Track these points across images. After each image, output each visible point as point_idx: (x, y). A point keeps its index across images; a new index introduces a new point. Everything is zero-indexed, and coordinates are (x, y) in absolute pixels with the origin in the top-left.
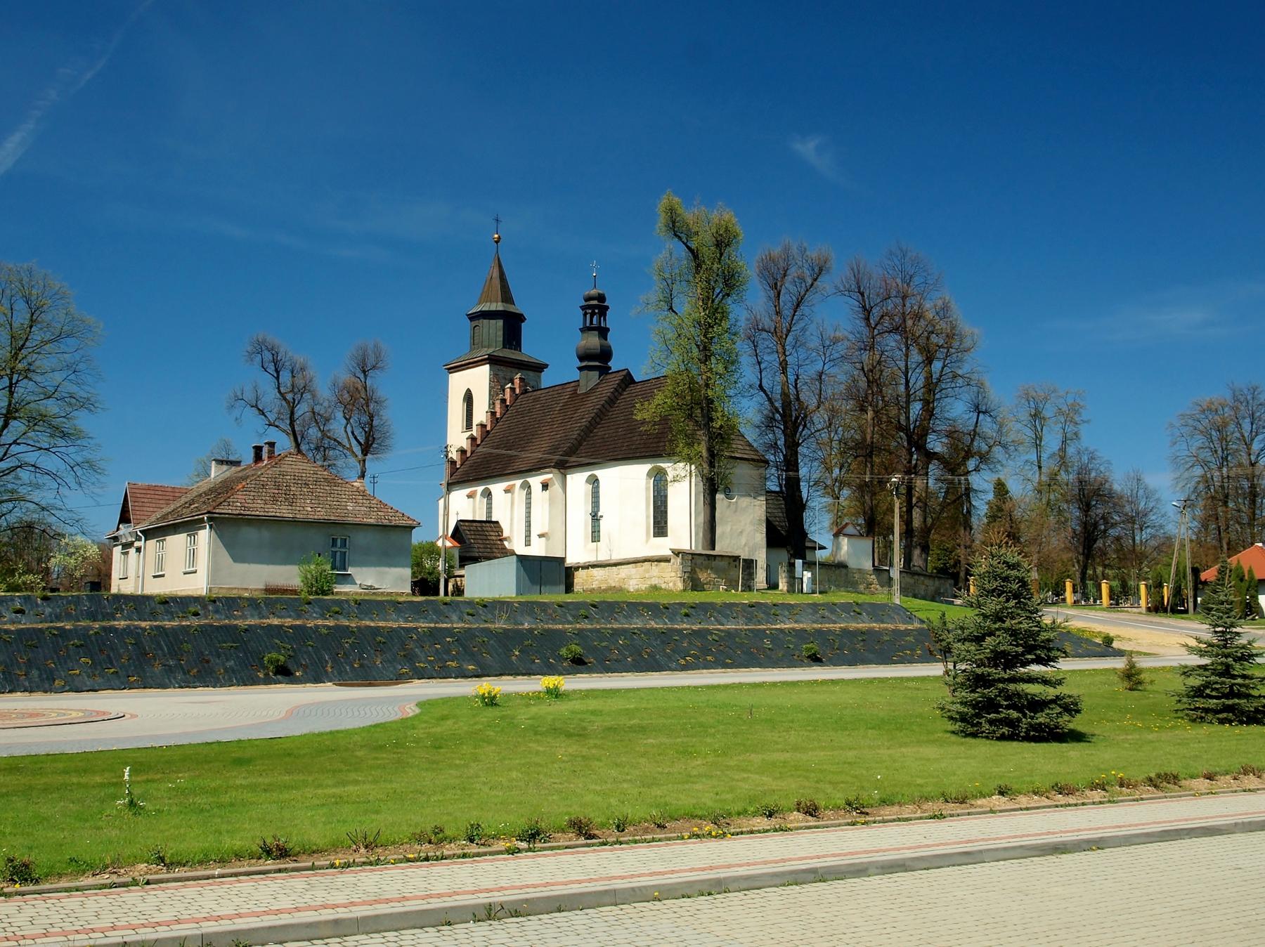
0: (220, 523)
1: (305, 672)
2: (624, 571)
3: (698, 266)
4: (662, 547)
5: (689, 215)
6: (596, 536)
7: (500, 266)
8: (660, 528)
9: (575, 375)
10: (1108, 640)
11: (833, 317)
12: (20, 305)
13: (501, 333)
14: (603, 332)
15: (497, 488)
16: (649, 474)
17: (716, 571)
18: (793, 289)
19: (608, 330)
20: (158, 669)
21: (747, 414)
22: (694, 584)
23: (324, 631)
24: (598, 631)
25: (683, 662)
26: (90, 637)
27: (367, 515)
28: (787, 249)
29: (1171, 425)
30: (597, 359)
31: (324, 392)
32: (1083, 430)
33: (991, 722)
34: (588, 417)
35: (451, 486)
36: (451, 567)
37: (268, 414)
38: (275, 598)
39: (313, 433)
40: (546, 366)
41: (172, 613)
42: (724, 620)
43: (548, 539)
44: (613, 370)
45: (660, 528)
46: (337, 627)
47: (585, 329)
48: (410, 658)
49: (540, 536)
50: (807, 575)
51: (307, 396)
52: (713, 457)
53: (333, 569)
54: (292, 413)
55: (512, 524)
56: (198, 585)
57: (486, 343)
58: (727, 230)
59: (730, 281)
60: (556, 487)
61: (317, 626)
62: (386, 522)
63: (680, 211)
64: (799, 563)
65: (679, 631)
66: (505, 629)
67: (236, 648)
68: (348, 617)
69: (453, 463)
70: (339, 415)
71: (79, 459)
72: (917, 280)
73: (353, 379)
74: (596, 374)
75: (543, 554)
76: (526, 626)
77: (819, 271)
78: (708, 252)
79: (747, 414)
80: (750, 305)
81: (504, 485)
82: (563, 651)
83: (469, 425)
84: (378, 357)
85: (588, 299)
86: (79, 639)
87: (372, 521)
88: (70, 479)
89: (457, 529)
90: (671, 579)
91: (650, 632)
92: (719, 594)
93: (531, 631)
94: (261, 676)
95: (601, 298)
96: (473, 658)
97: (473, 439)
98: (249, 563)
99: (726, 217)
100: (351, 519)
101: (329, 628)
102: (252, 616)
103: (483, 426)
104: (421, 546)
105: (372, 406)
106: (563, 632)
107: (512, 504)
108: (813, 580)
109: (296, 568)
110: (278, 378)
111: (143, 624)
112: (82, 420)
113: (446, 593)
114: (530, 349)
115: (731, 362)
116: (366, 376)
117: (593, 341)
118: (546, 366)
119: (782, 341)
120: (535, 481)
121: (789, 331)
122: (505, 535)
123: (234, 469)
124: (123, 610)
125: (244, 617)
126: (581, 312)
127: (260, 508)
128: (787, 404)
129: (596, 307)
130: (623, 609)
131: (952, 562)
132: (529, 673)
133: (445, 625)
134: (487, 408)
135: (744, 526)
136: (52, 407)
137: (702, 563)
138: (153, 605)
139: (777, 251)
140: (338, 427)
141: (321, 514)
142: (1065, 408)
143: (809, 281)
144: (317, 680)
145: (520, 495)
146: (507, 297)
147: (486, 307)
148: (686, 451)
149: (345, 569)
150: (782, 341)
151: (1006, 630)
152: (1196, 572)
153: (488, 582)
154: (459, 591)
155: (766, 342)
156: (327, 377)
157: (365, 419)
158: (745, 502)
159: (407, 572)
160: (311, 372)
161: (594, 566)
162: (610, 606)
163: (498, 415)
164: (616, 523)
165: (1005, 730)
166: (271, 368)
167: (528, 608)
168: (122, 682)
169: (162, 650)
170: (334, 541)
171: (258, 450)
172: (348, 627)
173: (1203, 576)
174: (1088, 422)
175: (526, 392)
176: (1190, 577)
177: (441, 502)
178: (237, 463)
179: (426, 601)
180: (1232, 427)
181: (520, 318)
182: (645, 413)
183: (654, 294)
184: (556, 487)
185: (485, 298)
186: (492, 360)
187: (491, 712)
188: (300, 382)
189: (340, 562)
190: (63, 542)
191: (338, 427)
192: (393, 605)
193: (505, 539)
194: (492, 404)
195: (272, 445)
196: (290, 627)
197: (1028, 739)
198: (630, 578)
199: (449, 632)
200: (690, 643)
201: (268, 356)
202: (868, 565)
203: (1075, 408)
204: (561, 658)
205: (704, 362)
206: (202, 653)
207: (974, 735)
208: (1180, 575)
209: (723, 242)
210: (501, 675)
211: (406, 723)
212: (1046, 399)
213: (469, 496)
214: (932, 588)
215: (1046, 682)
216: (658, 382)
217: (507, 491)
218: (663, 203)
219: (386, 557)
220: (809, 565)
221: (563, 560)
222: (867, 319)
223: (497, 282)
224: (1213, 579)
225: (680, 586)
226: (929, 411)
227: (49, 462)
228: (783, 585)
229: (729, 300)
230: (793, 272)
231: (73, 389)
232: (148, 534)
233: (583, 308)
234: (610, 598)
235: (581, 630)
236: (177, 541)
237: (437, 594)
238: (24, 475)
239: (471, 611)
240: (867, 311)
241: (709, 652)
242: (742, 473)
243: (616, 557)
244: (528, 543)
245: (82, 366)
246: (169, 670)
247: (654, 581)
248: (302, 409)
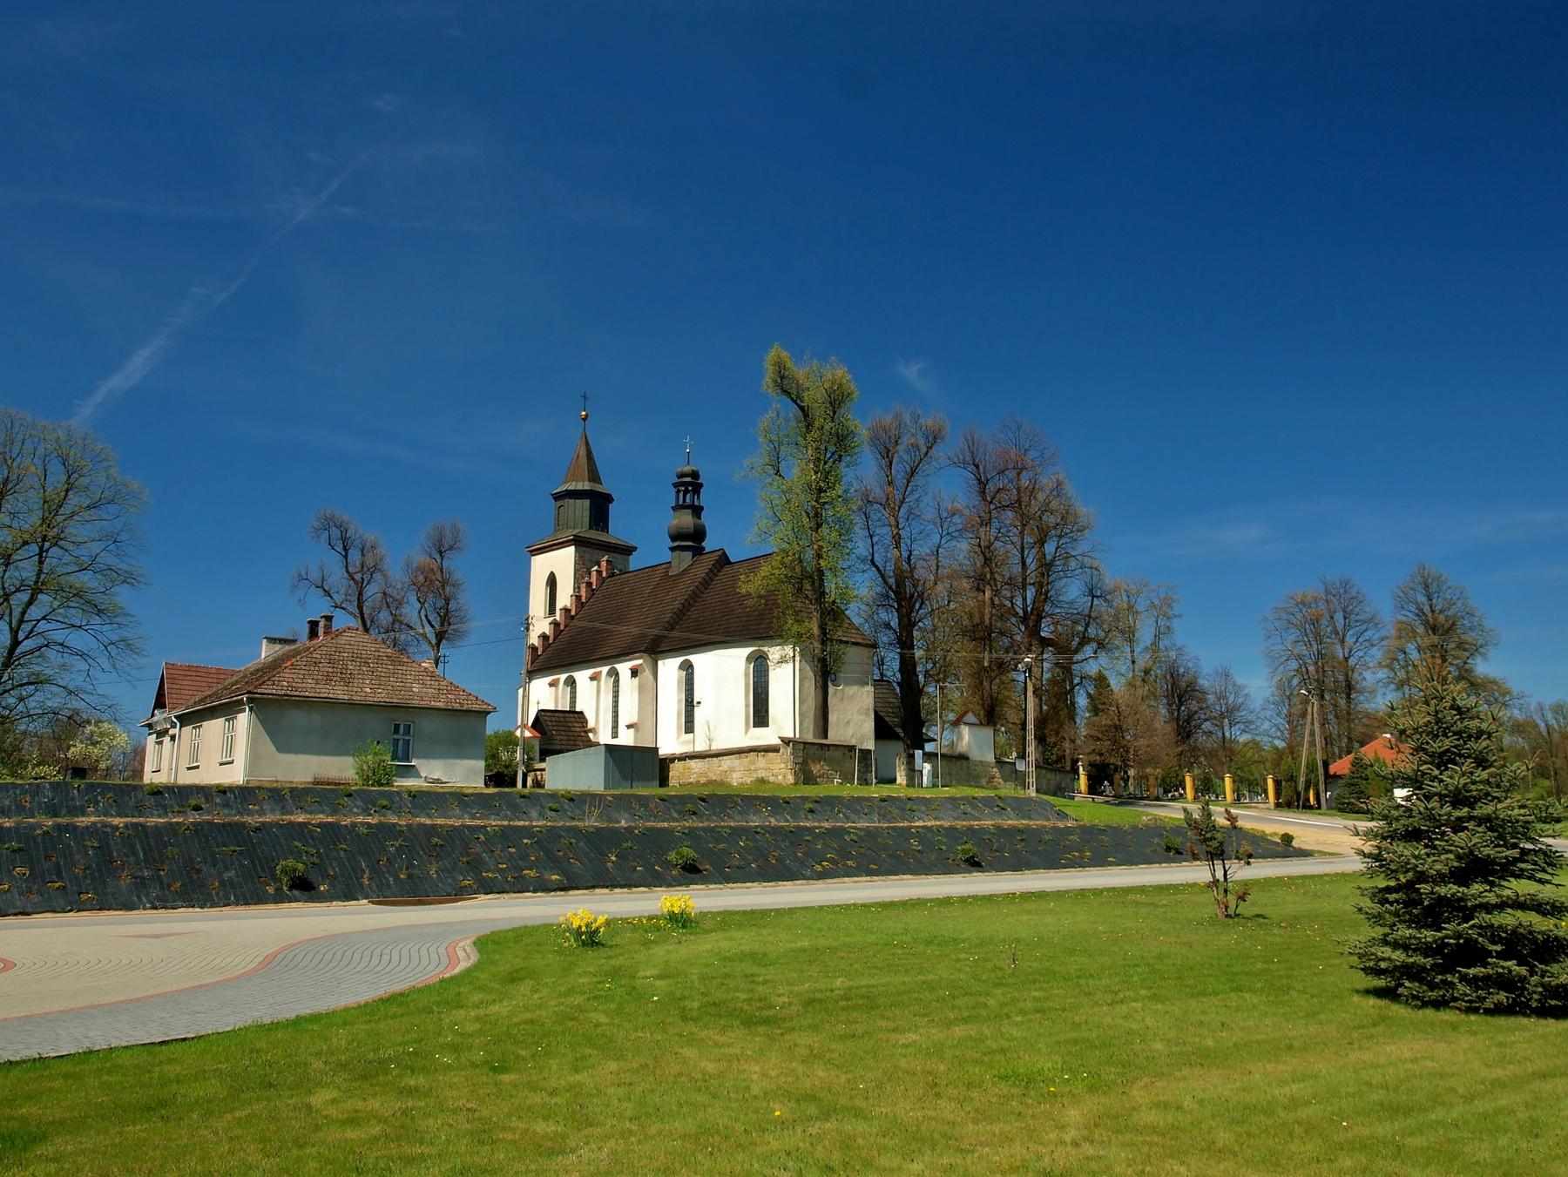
0: (260, 705)
1: (332, 885)
2: (727, 762)
3: (809, 426)
5: (800, 372)
7: (587, 444)
8: (761, 717)
9: (667, 556)
10: (1287, 839)
11: (947, 489)
12: (55, 467)
14: (697, 511)
15: (582, 676)
19: (702, 508)
20: (125, 881)
23: (364, 830)
24: (712, 830)
25: (819, 868)
26: (34, 838)
28: (898, 417)
29: (1266, 619)
31: (397, 574)
32: (1176, 624)
33: (1472, 982)
34: (681, 599)
35: (532, 674)
37: (335, 596)
38: (325, 793)
39: (385, 617)
41: (165, 808)
42: (853, 816)
45: (761, 717)
46: (381, 825)
48: (475, 866)
49: (629, 727)
50: (927, 767)
51: (377, 576)
52: (825, 639)
54: (360, 594)
56: (236, 775)
58: (840, 386)
59: (842, 441)
60: (647, 674)
61: (354, 825)
62: (457, 706)
63: (790, 364)
65: (810, 830)
66: (597, 828)
67: (240, 853)
68: (398, 813)
69: (534, 649)
70: (413, 598)
71: (114, 638)
75: (631, 743)
77: (934, 439)
78: (819, 412)
79: (859, 592)
80: (863, 472)
81: (590, 672)
82: (672, 856)
83: (552, 611)
84: (456, 539)
86: (19, 842)
87: (440, 705)
88: (103, 661)
90: (780, 772)
91: (774, 831)
92: (834, 787)
93: (629, 830)
94: (271, 890)
95: (695, 475)
96: (556, 863)
97: (556, 624)
98: (296, 752)
100: (415, 703)
101: (369, 825)
102: (273, 811)
103: (566, 610)
104: (497, 735)
106: (670, 831)
108: (934, 774)
109: (349, 760)
110: (346, 557)
111: (116, 821)
112: (123, 596)
113: (524, 785)
114: (618, 530)
115: (845, 530)
117: (686, 520)
120: (624, 668)
121: (902, 502)
122: (591, 724)
123: (287, 648)
124: (97, 803)
125: (262, 812)
127: (310, 688)
128: (900, 583)
129: (690, 485)
130: (736, 803)
132: (629, 884)
135: (854, 715)
136: (86, 580)
137: (812, 753)
138: (140, 796)
139: (888, 420)
140: (411, 611)
141: (382, 696)
142: (1157, 602)
143: (924, 450)
144: (348, 896)
145: (606, 684)
146: (594, 476)
147: (571, 486)
148: (796, 628)
151: (1481, 821)
152: (1326, 765)
153: (568, 774)
154: (538, 784)
155: (877, 513)
156: (400, 557)
157: (440, 603)
158: (853, 689)
159: (481, 764)
160: (383, 550)
162: (718, 800)
164: (718, 709)
165: (1502, 997)
166: (340, 547)
167: (623, 802)
168: (70, 901)
169: (135, 854)
170: (397, 727)
171: (314, 625)
173: (1333, 769)
174: (1180, 616)
175: (613, 575)
176: (1321, 771)
177: (521, 691)
178: (294, 641)
180: (1324, 622)
181: (608, 499)
182: (751, 585)
183: (759, 458)
186: (578, 542)
187: (593, 961)
188: (370, 562)
190: (89, 729)
191: (411, 611)
192: (462, 799)
194: (577, 588)
195: (329, 619)
196: (318, 826)
197: (1543, 1012)
198: (732, 770)
199: (527, 831)
200: (825, 844)
201: (335, 532)
202: (990, 758)
203: (1168, 602)
204: (668, 864)
206: (192, 861)
207: (1438, 1004)
208: (1311, 768)
209: (836, 401)
210: (594, 887)
211: (448, 992)
212: (1138, 593)
213: (551, 685)
215: (1538, 907)
219: (456, 747)
220: (929, 757)
222: (983, 493)
224: (1346, 771)
225: (791, 779)
226: (1043, 596)
227: (77, 640)
228: (901, 779)
230: (906, 440)
231: (111, 560)
232: (184, 720)
234: (706, 792)
235: (692, 830)
236: (214, 726)
237: (514, 784)
238: (51, 654)
240: (982, 484)
241: (848, 856)
243: (718, 745)
244: (615, 735)
245: (124, 536)
246: (141, 884)
247: (761, 774)
248: (372, 591)
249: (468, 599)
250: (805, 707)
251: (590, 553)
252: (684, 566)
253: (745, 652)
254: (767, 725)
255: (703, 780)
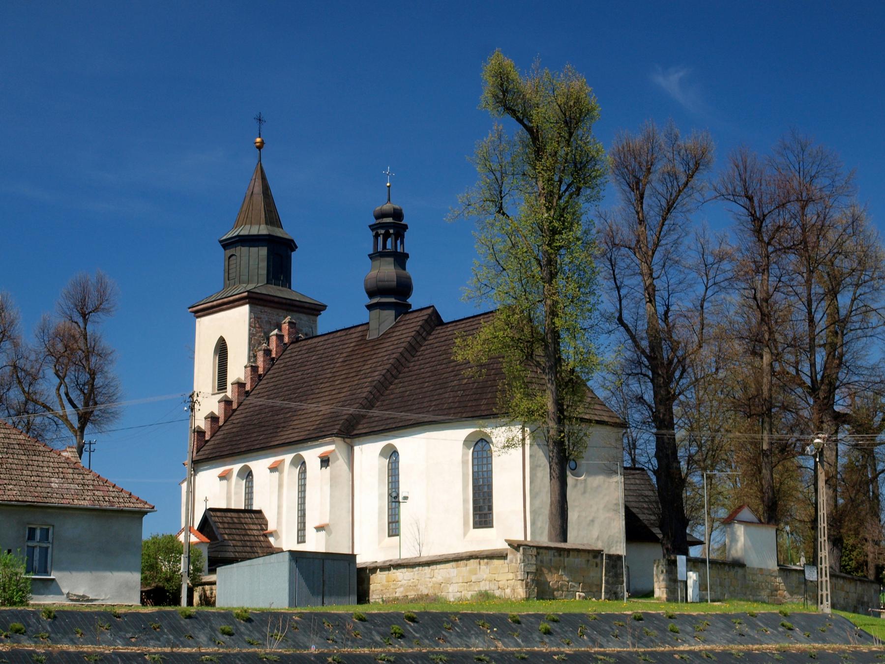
2: (441, 572)
4: (491, 539)
5: (526, 85)
6: (394, 528)
8: (483, 515)
9: (364, 316)
13: (264, 264)
14: (401, 259)
15: (260, 466)
16: (467, 442)
17: (571, 571)
18: (661, 189)
19: (406, 256)
21: (604, 357)
22: (540, 589)
27: (79, 495)
28: (650, 139)
30: (393, 295)
34: (381, 370)
35: (198, 464)
36: (198, 570)
40: (324, 307)
42: (600, 639)
43: (329, 533)
44: (414, 308)
45: (483, 515)
47: (376, 256)
49: (319, 529)
50: (693, 577)
53: (27, 572)
55: (279, 513)
57: (244, 278)
58: (578, 101)
59: (580, 171)
60: (340, 463)
62: (105, 505)
63: (514, 75)
64: (681, 559)
66: (281, 656)
68: (35, 637)
69: (200, 433)
70: (50, 372)
72: (822, 182)
73: (68, 324)
74: (390, 314)
75: (322, 550)
76: (313, 650)
78: (551, 132)
79: (604, 357)
80: (606, 208)
81: (269, 461)
84: (102, 296)
85: (380, 215)
87: (86, 504)
89: (205, 521)
90: (507, 583)
92: (576, 603)
97: (227, 402)
99: (576, 84)
100: (55, 501)
103: (240, 385)
104: (155, 541)
105: (93, 360)
107: (280, 486)
108: (702, 585)
113: (190, 602)
114: (304, 283)
116: (85, 321)
117: (387, 270)
118: (324, 307)
119: (647, 259)
120: (312, 455)
121: (657, 245)
122: (271, 527)
126: (371, 234)
128: (655, 346)
129: (391, 228)
130: (454, 624)
131: (853, 564)
133: (187, 650)
134: (245, 362)
135: (600, 514)
137: (549, 559)
139: (638, 141)
143: (683, 179)
145: (290, 474)
146: (272, 218)
147: (245, 231)
148: (525, 404)
149: (46, 572)
150: (647, 259)
154: (207, 601)
155: (626, 260)
157: (84, 377)
158: (597, 480)
159: (136, 577)
161: (398, 566)
163: (261, 371)
172: (31, 653)
177: (184, 486)
179: (160, 614)
181: (289, 245)
182: (469, 351)
183: (477, 191)
184: (340, 463)
185: (246, 218)
186: (253, 299)
189: (40, 563)
191: (48, 387)
192: (113, 620)
193: (271, 534)
194: (253, 356)
198: (449, 582)
205: (550, 282)
209: (573, 118)
213: (222, 477)
214: (853, 596)
216: (472, 322)
217: (273, 469)
218: (492, 64)
219: (104, 557)
220: (694, 564)
221: (353, 557)
222: (758, 231)
223: (259, 199)
225: (521, 592)
226: (837, 359)
228: (660, 591)
229: (581, 199)
230: (660, 167)
233: (373, 227)
237: (176, 601)
239: (228, 628)
240: (758, 221)
242: (598, 438)
243: (429, 552)
244: (301, 539)
247: (484, 587)
249: (119, 372)
250: (537, 503)
251: (269, 314)
252: (385, 327)
253: (463, 433)
254: (492, 527)
255: (412, 595)
